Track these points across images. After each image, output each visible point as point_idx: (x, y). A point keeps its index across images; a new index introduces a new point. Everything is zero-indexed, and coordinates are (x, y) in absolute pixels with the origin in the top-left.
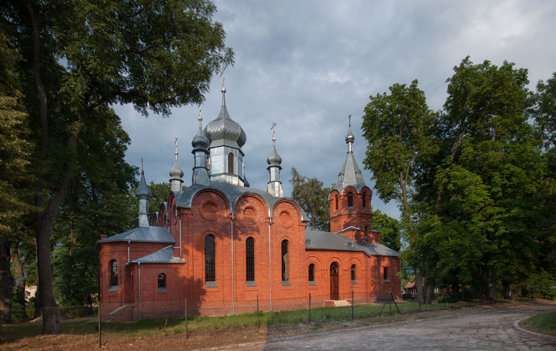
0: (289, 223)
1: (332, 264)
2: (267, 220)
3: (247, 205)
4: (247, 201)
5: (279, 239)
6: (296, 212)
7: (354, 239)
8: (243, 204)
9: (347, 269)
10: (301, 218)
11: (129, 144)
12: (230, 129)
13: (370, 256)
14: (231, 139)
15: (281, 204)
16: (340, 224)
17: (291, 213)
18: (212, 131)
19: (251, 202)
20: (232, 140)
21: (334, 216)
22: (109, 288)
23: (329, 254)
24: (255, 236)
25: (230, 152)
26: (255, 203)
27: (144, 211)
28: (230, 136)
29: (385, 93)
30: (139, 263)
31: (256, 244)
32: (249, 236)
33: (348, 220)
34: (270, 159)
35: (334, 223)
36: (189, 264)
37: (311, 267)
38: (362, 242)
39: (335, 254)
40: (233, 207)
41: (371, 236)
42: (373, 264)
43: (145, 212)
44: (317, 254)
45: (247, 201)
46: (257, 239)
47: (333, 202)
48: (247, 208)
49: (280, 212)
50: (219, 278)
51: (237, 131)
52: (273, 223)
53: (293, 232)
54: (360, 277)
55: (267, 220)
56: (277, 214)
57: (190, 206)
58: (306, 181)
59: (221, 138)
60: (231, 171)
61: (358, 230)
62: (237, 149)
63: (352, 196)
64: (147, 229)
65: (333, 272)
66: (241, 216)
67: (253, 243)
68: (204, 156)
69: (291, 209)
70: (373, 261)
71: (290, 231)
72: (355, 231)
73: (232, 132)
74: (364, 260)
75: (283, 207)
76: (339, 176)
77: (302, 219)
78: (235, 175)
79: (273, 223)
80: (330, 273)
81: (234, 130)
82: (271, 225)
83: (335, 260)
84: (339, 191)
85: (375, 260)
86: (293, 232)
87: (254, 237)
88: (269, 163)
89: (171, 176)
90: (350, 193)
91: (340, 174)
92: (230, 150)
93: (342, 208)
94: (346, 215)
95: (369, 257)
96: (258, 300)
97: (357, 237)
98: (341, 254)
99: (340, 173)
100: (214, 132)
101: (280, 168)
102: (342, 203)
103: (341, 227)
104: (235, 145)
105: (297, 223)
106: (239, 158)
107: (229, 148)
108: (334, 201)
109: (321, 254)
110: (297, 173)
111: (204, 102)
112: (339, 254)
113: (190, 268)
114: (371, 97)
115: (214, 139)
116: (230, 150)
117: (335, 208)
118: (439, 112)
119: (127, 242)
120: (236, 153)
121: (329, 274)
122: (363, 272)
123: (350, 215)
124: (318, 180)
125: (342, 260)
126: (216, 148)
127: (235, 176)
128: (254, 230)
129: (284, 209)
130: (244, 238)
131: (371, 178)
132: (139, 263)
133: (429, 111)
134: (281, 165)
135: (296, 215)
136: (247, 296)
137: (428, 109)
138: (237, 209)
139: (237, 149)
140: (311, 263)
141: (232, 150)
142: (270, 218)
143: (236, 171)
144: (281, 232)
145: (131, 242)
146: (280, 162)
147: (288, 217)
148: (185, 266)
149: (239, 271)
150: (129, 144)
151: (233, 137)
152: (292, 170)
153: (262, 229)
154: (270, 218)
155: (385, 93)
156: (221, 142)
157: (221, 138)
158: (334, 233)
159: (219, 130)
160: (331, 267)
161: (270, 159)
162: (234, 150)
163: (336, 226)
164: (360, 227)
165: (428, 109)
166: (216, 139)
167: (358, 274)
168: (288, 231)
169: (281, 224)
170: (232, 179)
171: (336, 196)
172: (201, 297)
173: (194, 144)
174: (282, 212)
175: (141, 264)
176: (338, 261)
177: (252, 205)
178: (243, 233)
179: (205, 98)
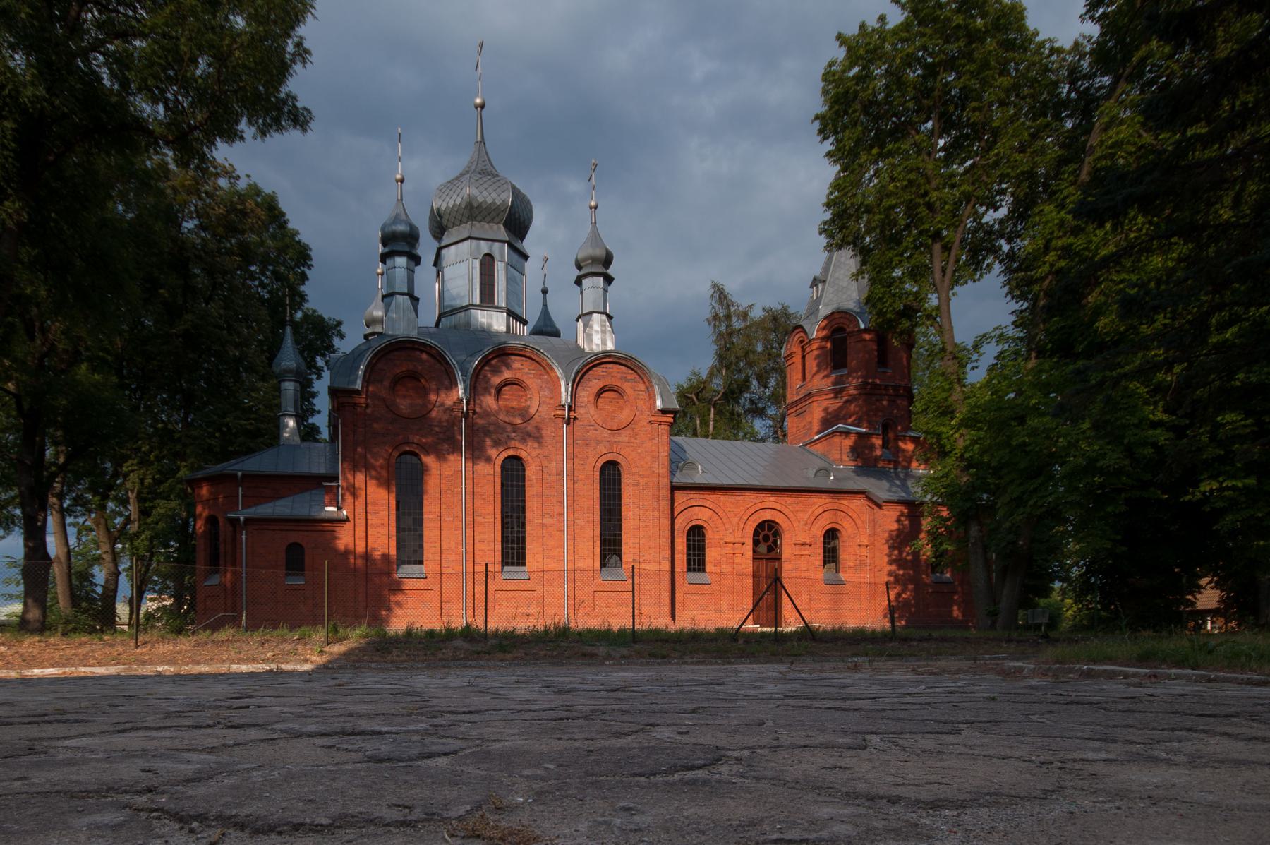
0: (625, 416)
1: (761, 526)
2: (559, 412)
3: (507, 375)
4: (509, 367)
5: (592, 460)
6: (642, 386)
7: (845, 458)
8: (496, 371)
9: (808, 541)
10: (655, 403)
11: (310, 267)
12: (485, 194)
13: (880, 502)
14: (479, 218)
15: (598, 370)
16: (809, 420)
17: (629, 391)
18: (443, 208)
19: (519, 369)
20: (492, 221)
21: (795, 399)
22: (206, 579)
23: (750, 499)
24: (527, 452)
25: (486, 252)
26: (526, 370)
27: (289, 409)
28: (494, 214)
29: (882, 19)
30: (242, 518)
31: (531, 472)
32: (510, 452)
33: (835, 405)
34: (579, 257)
35: (796, 419)
36: (358, 521)
37: (696, 535)
38: (875, 466)
39: (771, 500)
40: (464, 381)
41: (910, 447)
42: (895, 526)
43: (292, 410)
44: (710, 499)
45: (509, 367)
46: (531, 461)
47: (793, 360)
48: (507, 383)
49: (595, 390)
50: (431, 557)
51: (504, 196)
52: (575, 418)
53: (633, 440)
54: (852, 564)
55: (559, 412)
56: (586, 394)
57: (358, 385)
58: (757, 314)
59: (465, 219)
60: (488, 299)
61: (859, 434)
62: (503, 242)
63: (845, 339)
64: (295, 447)
65: (763, 548)
66: (489, 401)
67: (524, 470)
68: (405, 265)
69: (629, 381)
70: (895, 518)
71: (624, 437)
72: (853, 437)
73: (489, 201)
74: (866, 518)
75: (603, 377)
76: (812, 287)
77: (659, 404)
78: (498, 307)
79: (575, 418)
80: (754, 552)
81: (494, 195)
82: (568, 424)
83: (768, 515)
84: (807, 328)
85: (902, 514)
86: (633, 440)
87: (523, 454)
88: (579, 267)
89: (368, 327)
90: (840, 330)
91: (815, 282)
92: (484, 247)
93: (818, 372)
94: (826, 392)
95: (880, 506)
96: (367, 573)
97: (860, 451)
98: (789, 500)
99: (815, 279)
100: (447, 207)
101: (609, 280)
102: (817, 357)
103: (810, 429)
104: (502, 233)
105: (645, 417)
106: (508, 264)
107: (482, 242)
108: (797, 359)
109: (726, 500)
110: (726, 297)
111: (312, 125)
112: (782, 500)
113: (360, 532)
114: (839, 36)
115: (458, 223)
116: (484, 247)
117: (800, 376)
118: (1081, 39)
119: (236, 475)
120: (501, 252)
121: (750, 554)
122: (864, 551)
123: (837, 393)
124: (791, 311)
125: (791, 515)
126: (453, 247)
127: (498, 309)
128: (526, 436)
129: (608, 381)
130: (498, 456)
131: (853, 275)
132: (242, 518)
133: (1042, 44)
134: (611, 271)
135: (643, 395)
136: (505, 603)
137: (1039, 39)
138: (476, 385)
139: (503, 242)
140: (694, 523)
141: (491, 248)
142: (564, 406)
143: (501, 298)
144: (598, 442)
145: (243, 476)
146: (607, 260)
147: (621, 401)
148: (347, 525)
149: (482, 541)
150: (309, 269)
151: (494, 214)
152: (711, 291)
153: (547, 432)
154: (564, 406)
155: (882, 19)
156: (464, 230)
157: (465, 219)
158: (794, 445)
159: (458, 202)
160: (756, 533)
161: (579, 257)
162: (497, 245)
163: (801, 425)
164: (871, 425)
165: (1039, 39)
166: (454, 225)
167: (626, 513)
168: (620, 439)
169: (599, 421)
170: (491, 317)
171: (802, 342)
172: (393, 598)
173: (385, 240)
174: (603, 390)
175: (246, 520)
176: (779, 518)
177: (518, 376)
178: (497, 444)
179: (313, 114)
